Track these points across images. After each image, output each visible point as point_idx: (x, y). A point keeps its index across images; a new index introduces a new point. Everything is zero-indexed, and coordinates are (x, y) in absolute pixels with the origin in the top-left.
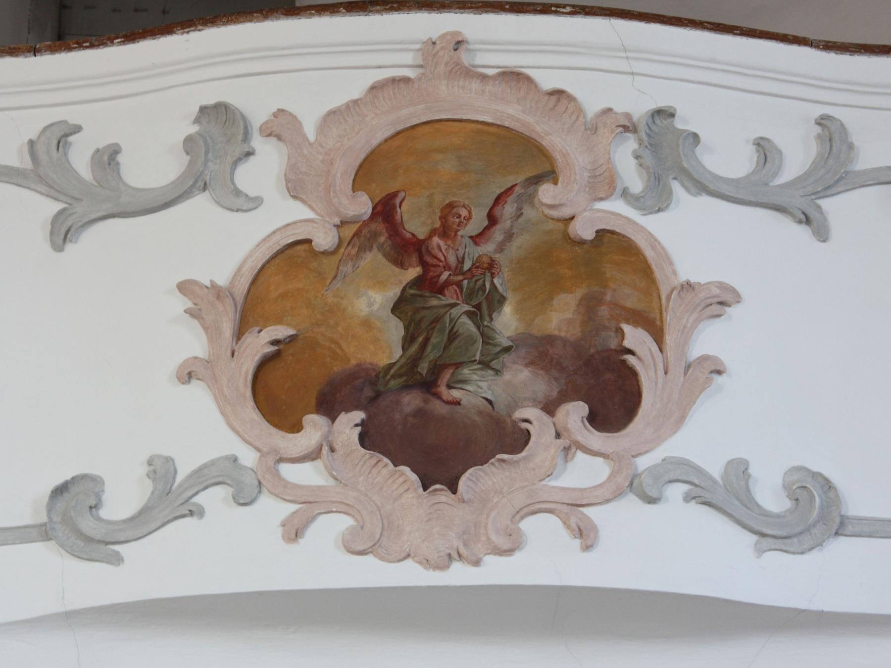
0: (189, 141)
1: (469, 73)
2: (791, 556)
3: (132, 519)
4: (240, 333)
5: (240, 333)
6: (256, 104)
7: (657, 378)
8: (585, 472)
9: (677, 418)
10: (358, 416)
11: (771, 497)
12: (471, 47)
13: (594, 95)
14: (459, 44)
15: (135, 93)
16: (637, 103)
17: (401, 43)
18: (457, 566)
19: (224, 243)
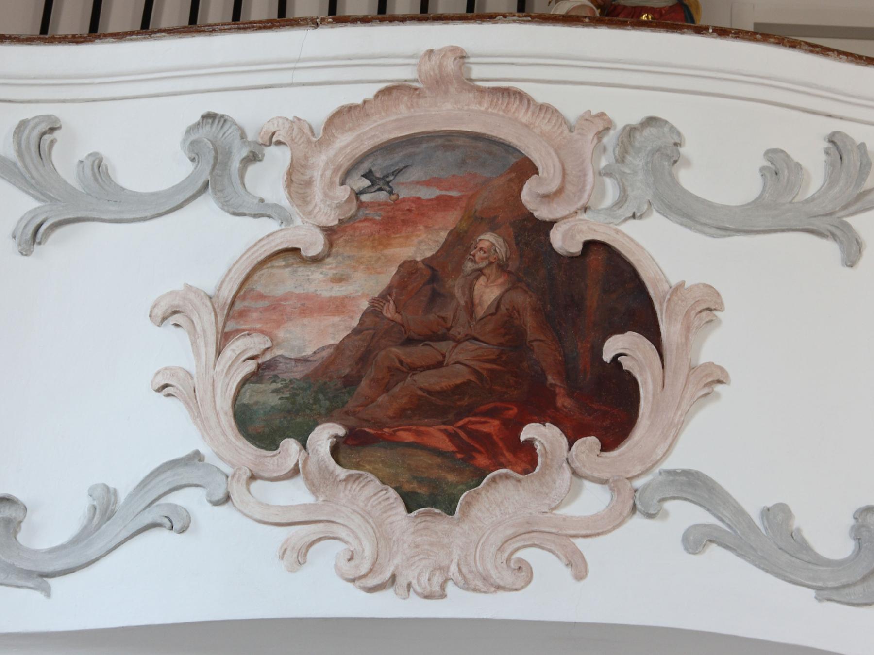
0: (763, 169)
1: (468, 84)
2: (609, 535)
3: (63, 547)
4: (224, 338)
5: (224, 338)
6: (251, 112)
7: (682, 398)
8: (593, 499)
9: (672, 433)
10: (341, 431)
11: (833, 542)
12: (472, 60)
13: (572, 103)
14: (463, 57)
15: (134, 101)
16: (626, 111)
17: (278, 62)
18: (388, 595)
19: (213, 246)
